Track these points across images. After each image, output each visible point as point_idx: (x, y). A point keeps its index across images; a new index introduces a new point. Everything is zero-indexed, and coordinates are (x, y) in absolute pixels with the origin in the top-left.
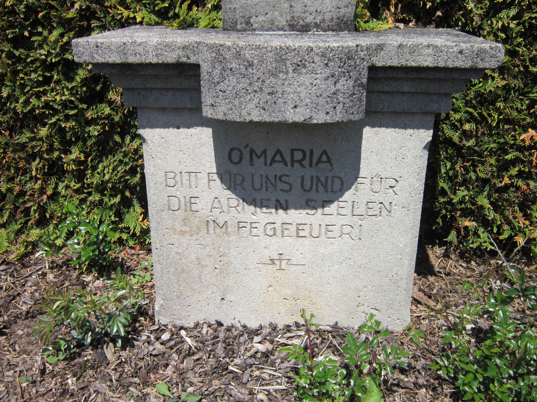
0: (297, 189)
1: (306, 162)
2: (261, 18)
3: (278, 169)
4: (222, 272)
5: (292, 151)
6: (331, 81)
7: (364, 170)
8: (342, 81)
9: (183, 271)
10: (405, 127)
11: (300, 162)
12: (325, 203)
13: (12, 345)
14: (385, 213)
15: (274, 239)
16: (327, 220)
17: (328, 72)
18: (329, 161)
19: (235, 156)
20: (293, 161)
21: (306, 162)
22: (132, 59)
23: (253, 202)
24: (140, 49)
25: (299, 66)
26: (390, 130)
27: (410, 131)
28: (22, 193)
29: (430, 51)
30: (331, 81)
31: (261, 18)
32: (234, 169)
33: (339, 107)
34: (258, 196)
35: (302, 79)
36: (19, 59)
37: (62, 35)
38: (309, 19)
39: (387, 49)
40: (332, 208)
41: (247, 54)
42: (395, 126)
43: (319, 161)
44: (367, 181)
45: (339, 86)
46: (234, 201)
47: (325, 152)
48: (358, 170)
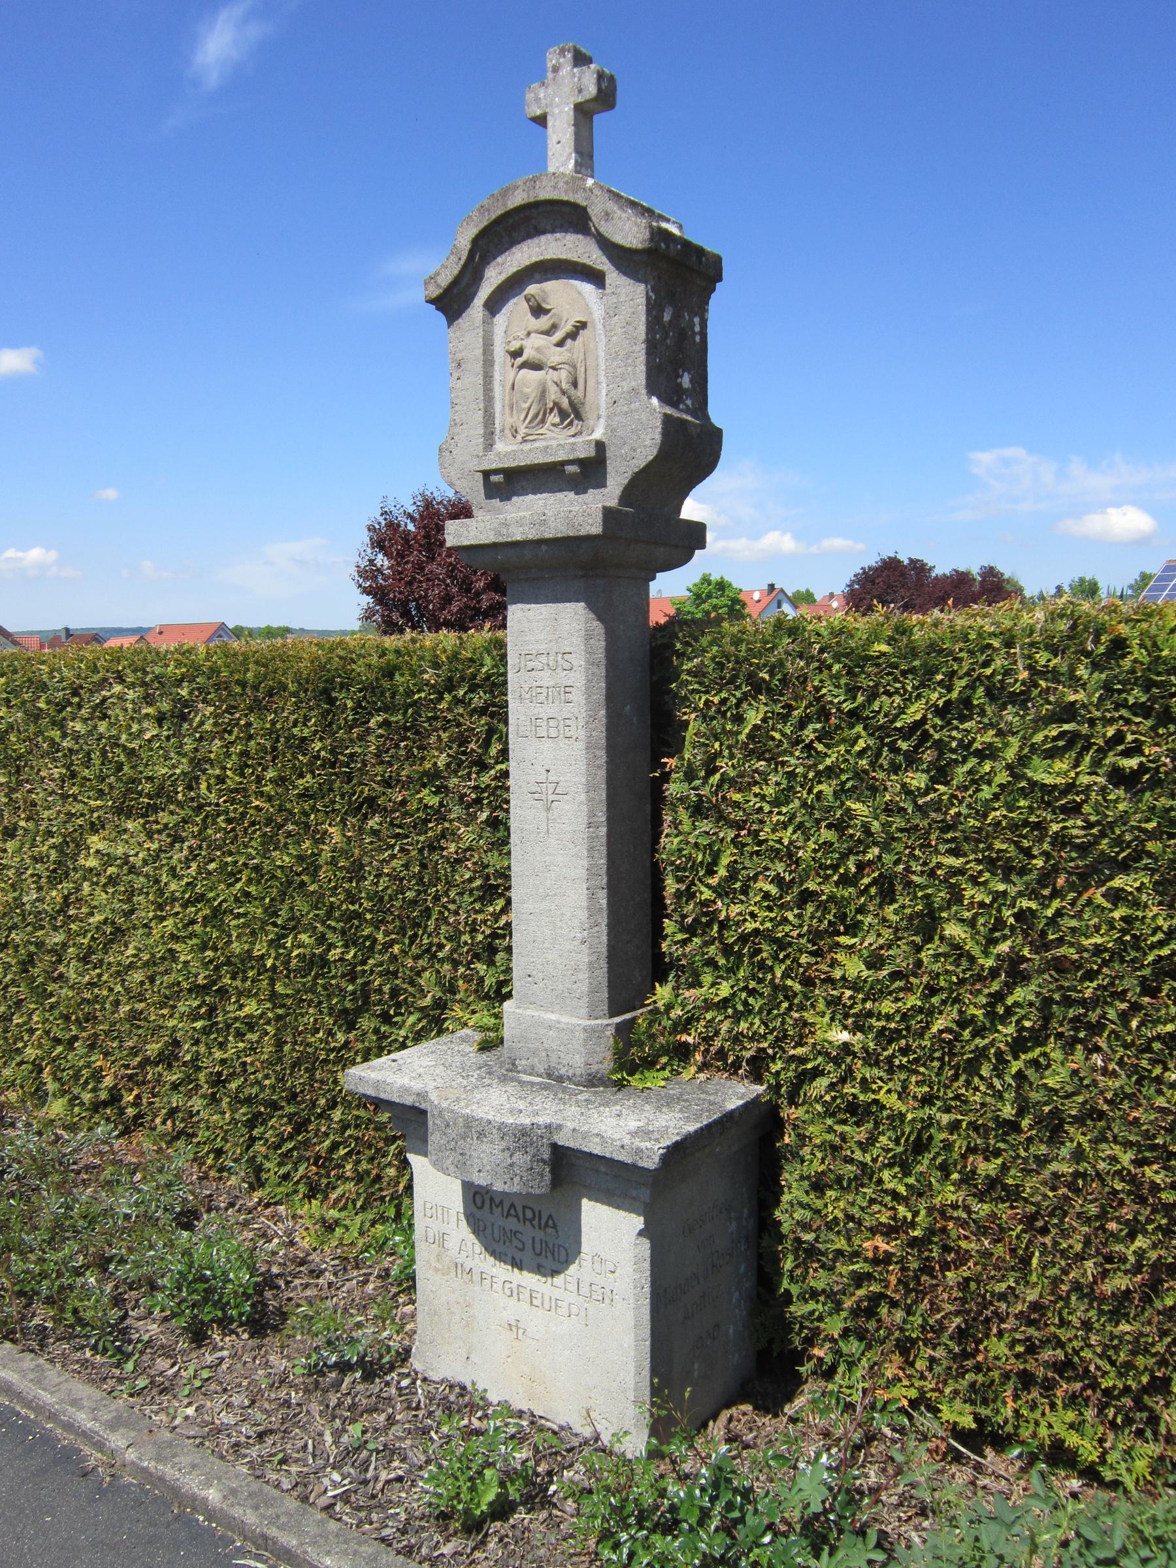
0: (529, 1251)
1: (536, 1222)
2: (524, 1062)
3: (512, 1224)
4: (467, 1325)
5: (524, 1207)
6: (507, 1154)
7: (585, 1248)
8: (518, 1155)
9: (435, 1313)
10: (618, 1207)
11: (531, 1221)
12: (554, 1273)
13: (282, 1347)
14: (607, 1301)
15: (513, 1302)
16: (557, 1294)
17: (504, 1144)
18: (555, 1226)
19: (478, 1199)
20: (525, 1219)
21: (536, 1222)
22: (383, 1096)
23: (493, 1253)
24: (388, 1088)
25: (481, 1135)
26: (605, 1207)
27: (622, 1213)
28: (378, 1178)
29: (597, 1140)
30: (507, 1154)
31: (524, 1062)
32: (478, 1213)
33: (517, 1180)
34: (499, 1248)
35: (484, 1147)
36: (384, 1037)
37: (419, 1020)
38: (563, 1071)
39: (565, 1130)
40: (559, 1280)
41: (447, 1115)
42: (609, 1204)
43: (547, 1225)
44: (588, 1258)
45: (514, 1159)
46: (478, 1248)
47: (550, 1217)
48: (579, 1243)
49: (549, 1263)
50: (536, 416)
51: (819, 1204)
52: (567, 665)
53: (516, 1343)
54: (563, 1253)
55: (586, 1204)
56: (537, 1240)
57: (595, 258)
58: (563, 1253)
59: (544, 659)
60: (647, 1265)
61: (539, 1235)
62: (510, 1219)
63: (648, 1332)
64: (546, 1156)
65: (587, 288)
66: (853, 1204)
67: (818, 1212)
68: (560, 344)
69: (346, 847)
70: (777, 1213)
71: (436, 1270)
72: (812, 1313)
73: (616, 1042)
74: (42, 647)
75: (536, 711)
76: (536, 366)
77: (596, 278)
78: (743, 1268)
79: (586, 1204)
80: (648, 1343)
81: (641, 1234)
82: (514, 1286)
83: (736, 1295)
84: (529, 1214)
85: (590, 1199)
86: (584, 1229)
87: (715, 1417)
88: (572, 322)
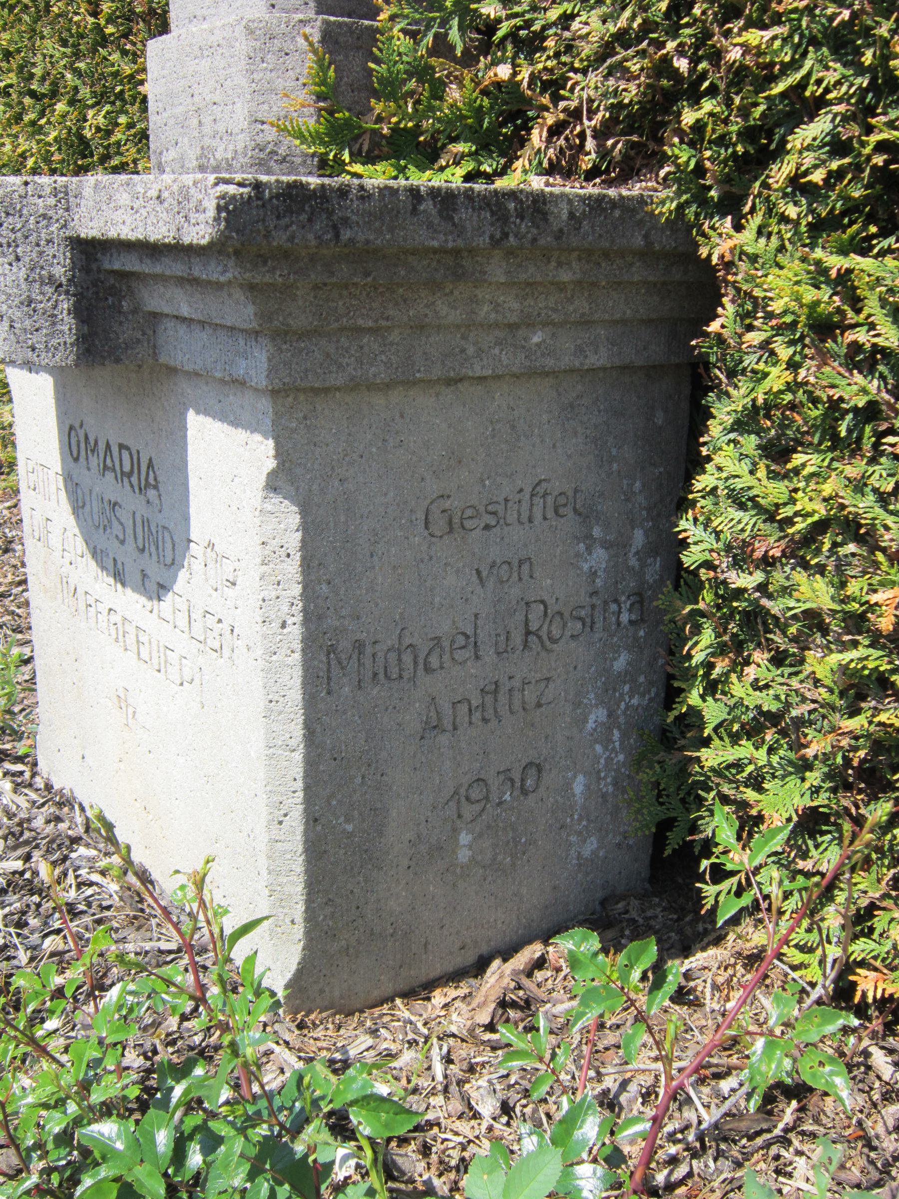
1: (134, 479)
10: (236, 423)
23: (97, 553)
49: (127, 554)
51: (776, 491)
55: (195, 422)
60: (292, 568)
63: (297, 731)
64: (59, 272)
66: (859, 486)
67: (770, 515)
70: (683, 524)
72: (738, 765)
73: (323, 67)
74: (279, 120)
78: (621, 663)
79: (195, 422)
80: (298, 756)
81: (273, 485)
83: (599, 715)
85: (198, 412)
86: (192, 484)
87: (507, 955)
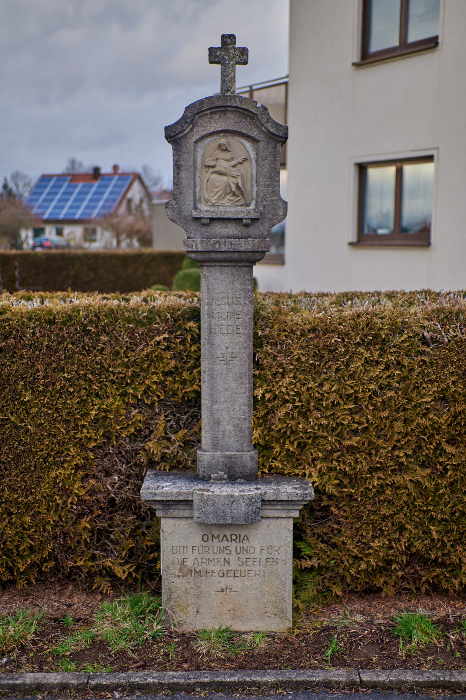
1: (237, 540)
4: (197, 597)
5: (231, 535)
11: (235, 540)
18: (248, 539)
20: (231, 540)
21: (237, 540)
50: (221, 195)
52: (237, 303)
53: (226, 596)
54: (252, 549)
56: (238, 548)
57: (255, 133)
58: (252, 549)
59: (226, 300)
61: (239, 545)
62: (224, 542)
65: (248, 145)
68: (234, 166)
69: (310, 400)
71: (179, 576)
75: (221, 322)
76: (220, 173)
77: (253, 140)
82: (225, 572)
84: (234, 537)
88: (242, 158)
